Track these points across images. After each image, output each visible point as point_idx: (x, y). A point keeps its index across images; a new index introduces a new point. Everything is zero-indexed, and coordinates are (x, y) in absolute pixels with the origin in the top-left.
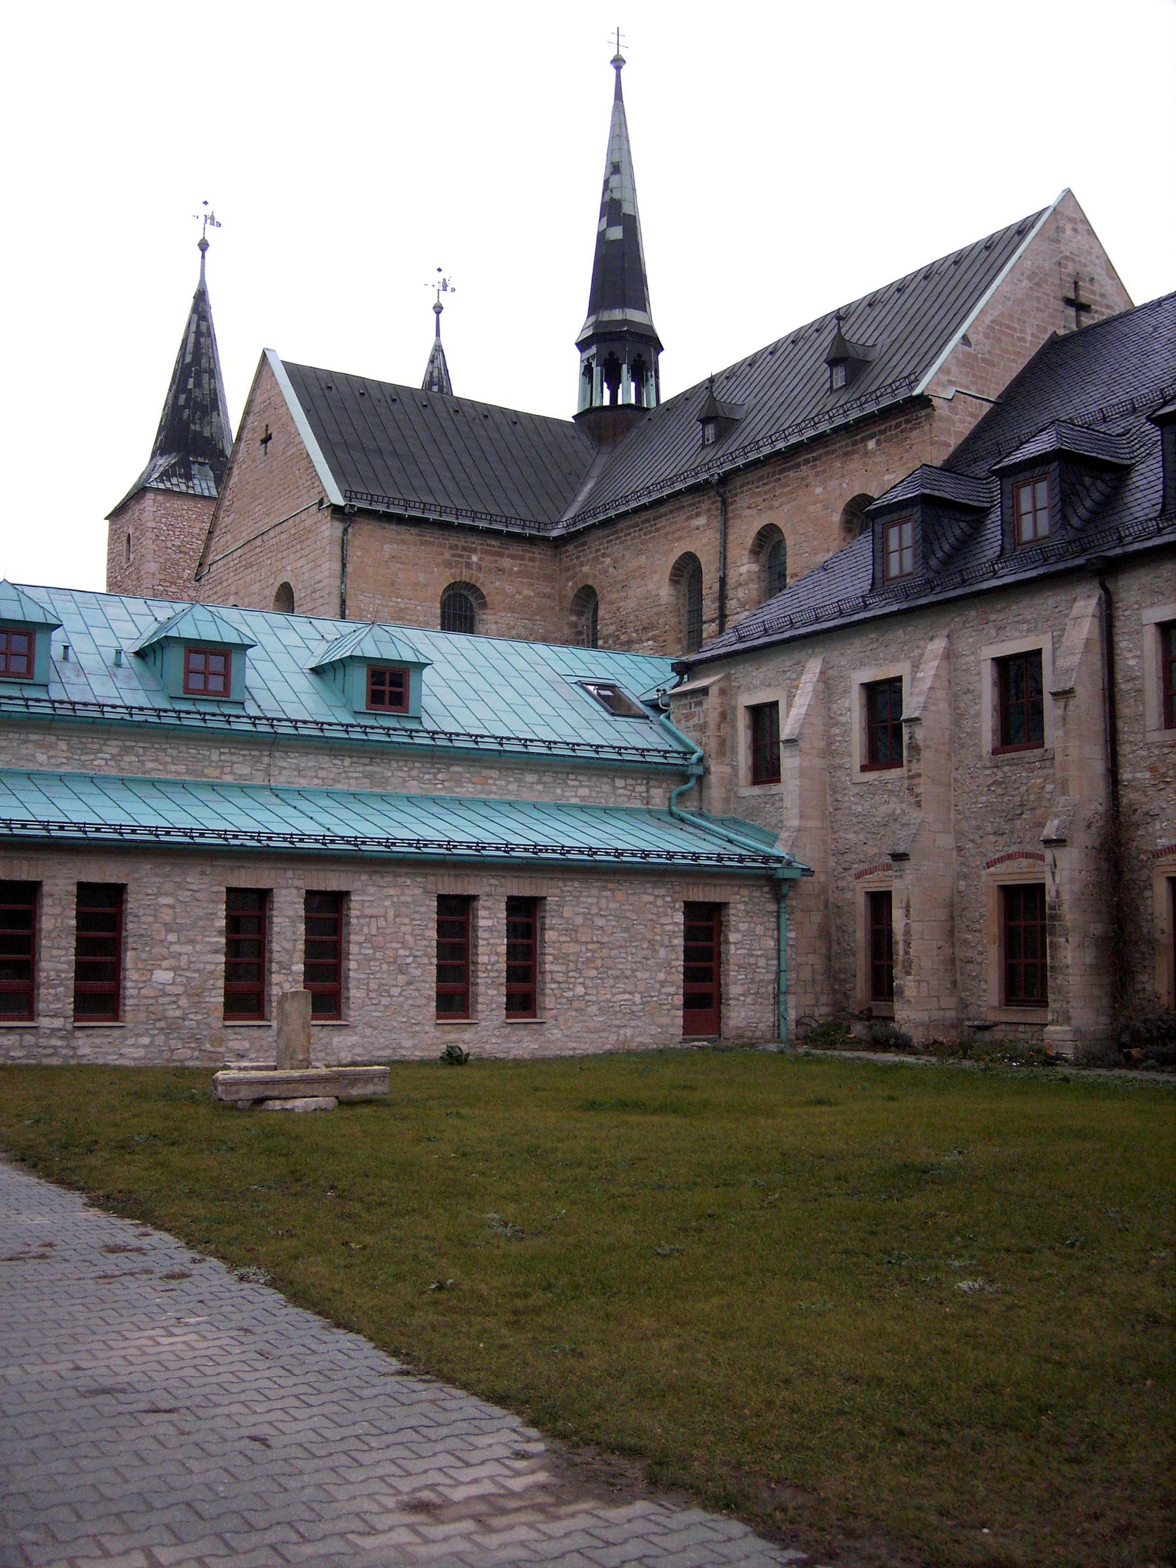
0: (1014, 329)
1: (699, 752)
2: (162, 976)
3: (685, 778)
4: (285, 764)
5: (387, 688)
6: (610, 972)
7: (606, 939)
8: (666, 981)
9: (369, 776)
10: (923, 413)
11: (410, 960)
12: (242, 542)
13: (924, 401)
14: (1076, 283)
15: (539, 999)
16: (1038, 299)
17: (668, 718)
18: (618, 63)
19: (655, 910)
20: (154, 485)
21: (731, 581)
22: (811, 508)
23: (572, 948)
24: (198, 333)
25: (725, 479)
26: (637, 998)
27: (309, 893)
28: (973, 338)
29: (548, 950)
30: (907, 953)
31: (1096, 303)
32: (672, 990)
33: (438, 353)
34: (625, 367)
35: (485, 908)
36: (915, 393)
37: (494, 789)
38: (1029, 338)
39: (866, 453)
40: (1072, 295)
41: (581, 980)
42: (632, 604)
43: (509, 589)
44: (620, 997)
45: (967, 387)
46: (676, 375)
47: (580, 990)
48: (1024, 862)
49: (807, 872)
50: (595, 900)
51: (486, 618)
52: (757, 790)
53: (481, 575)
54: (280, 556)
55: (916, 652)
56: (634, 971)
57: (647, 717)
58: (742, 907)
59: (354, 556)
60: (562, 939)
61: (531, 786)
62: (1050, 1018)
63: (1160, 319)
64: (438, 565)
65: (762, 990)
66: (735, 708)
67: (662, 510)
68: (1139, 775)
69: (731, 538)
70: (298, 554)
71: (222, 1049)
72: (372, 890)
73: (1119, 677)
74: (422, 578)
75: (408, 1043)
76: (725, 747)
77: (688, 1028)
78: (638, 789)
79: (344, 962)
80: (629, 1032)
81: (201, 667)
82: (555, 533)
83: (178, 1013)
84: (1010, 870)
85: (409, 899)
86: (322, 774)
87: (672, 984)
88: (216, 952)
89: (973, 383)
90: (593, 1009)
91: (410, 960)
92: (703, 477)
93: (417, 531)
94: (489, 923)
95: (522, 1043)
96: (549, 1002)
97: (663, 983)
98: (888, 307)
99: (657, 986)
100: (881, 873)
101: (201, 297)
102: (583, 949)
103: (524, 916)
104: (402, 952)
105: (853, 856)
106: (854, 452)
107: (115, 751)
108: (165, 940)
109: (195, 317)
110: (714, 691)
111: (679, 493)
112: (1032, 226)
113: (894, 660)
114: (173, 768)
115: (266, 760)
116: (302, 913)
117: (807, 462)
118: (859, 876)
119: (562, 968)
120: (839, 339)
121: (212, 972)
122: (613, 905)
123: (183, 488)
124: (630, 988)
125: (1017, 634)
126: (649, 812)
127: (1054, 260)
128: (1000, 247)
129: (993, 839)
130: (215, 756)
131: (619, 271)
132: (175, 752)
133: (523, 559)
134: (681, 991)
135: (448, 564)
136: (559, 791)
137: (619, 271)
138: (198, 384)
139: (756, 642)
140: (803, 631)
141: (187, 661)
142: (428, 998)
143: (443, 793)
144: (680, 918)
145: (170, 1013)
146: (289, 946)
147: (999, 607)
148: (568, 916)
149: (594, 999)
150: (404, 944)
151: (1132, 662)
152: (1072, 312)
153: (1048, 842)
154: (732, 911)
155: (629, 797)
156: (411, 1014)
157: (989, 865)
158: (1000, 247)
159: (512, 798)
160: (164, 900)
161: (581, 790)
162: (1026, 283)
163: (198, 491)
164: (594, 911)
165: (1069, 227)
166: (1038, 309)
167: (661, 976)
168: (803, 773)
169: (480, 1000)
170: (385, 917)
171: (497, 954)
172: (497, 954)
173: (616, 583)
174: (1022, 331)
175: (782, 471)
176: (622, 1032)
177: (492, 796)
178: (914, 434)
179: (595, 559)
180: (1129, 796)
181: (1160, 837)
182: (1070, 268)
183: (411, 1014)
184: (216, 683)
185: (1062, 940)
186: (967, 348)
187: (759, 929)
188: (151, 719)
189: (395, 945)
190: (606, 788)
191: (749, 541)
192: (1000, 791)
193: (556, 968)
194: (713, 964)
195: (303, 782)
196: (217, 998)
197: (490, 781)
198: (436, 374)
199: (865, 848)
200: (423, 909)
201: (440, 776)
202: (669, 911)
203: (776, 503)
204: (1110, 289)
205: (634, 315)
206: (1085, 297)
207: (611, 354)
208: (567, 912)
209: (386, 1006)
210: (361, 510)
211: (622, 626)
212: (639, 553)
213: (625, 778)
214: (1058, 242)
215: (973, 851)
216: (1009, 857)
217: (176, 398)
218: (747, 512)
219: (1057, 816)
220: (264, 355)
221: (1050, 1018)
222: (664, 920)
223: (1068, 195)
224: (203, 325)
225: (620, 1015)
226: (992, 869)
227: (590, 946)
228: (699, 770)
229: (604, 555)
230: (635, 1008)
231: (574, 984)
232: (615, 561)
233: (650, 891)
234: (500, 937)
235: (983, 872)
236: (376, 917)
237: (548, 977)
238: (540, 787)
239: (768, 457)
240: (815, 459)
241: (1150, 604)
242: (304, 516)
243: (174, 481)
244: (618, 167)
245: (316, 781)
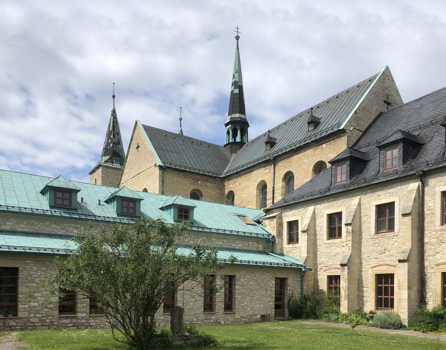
0: (370, 110)
5: (183, 214)
7: (253, 288)
12: (131, 177)
14: (388, 96)
15: (233, 306)
16: (377, 101)
17: (262, 225)
18: (237, 38)
20: (103, 164)
22: (303, 166)
23: (244, 291)
24: (114, 122)
28: (358, 111)
29: (236, 291)
31: (393, 103)
32: (272, 303)
34: (239, 131)
36: (341, 128)
39: (322, 148)
40: (386, 100)
46: (253, 133)
47: (246, 303)
48: (386, 267)
49: (310, 270)
50: (250, 277)
52: (291, 246)
54: (143, 181)
55: (348, 204)
56: (261, 298)
57: (256, 225)
59: (166, 180)
60: (241, 288)
63: (423, 103)
68: (432, 240)
70: (149, 180)
74: (185, 187)
76: (280, 233)
78: (255, 245)
79: (176, 295)
82: (222, 176)
84: (380, 269)
87: (272, 302)
92: (267, 158)
93: (183, 174)
96: (237, 307)
97: (269, 302)
98: (324, 107)
100: (333, 270)
103: (230, 281)
105: (323, 265)
109: (112, 117)
111: (261, 163)
112: (375, 78)
113: (340, 206)
118: (325, 271)
119: (241, 297)
120: (312, 116)
123: (111, 166)
124: (260, 303)
125: (386, 197)
128: (363, 86)
129: (374, 260)
131: (237, 101)
138: (114, 137)
139: (291, 203)
140: (315, 197)
141: (122, 204)
142: (201, 306)
147: (379, 189)
148: (243, 281)
151: (431, 204)
156: (196, 311)
158: (363, 86)
163: (115, 167)
165: (387, 78)
167: (268, 299)
169: (217, 306)
173: (240, 190)
174: (372, 110)
181: (440, 260)
182: (387, 91)
183: (196, 311)
184: (131, 211)
188: (111, 220)
191: (282, 176)
192: (377, 245)
193: (238, 297)
194: (282, 296)
199: (327, 263)
203: (291, 165)
204: (397, 99)
208: (242, 280)
211: (242, 202)
212: (247, 181)
215: (367, 264)
216: (380, 265)
217: (108, 141)
220: (136, 123)
222: (269, 283)
223: (387, 68)
226: (373, 269)
227: (248, 290)
229: (236, 182)
237: (236, 299)
239: (289, 151)
241: (439, 185)
242: (150, 169)
243: (108, 163)
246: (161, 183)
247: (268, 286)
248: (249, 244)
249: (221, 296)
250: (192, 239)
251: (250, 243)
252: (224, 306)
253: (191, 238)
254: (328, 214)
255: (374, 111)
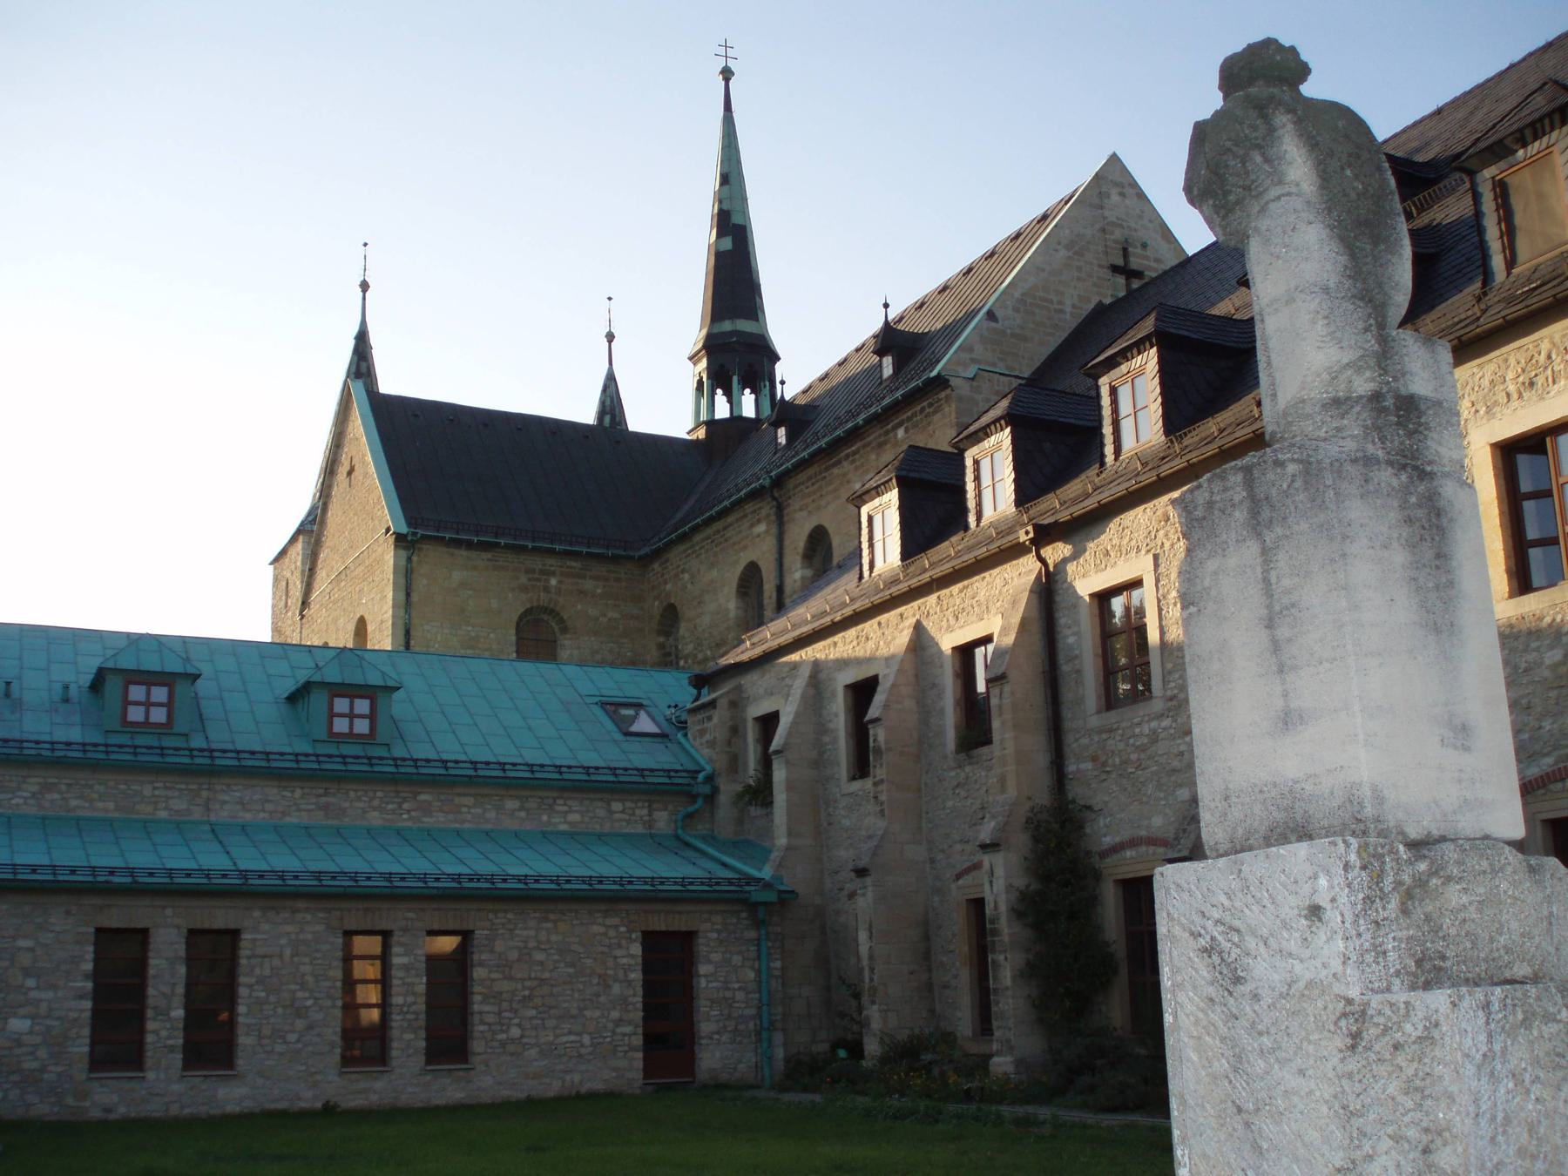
0: (1051, 301)
1: (708, 768)
2: (18, 1025)
3: (693, 798)
4: (226, 798)
6: (552, 1012)
7: (546, 975)
8: (621, 1020)
9: (325, 807)
10: (943, 395)
11: (309, 1003)
13: (941, 382)
14: (1125, 250)
16: (1079, 269)
17: (685, 735)
19: (607, 941)
21: (788, 589)
23: (506, 986)
25: (778, 482)
26: (586, 1040)
27: (192, 933)
28: (999, 313)
29: (477, 989)
30: (872, 980)
32: (628, 1029)
33: (610, 383)
35: (401, 944)
37: (469, 817)
38: (1068, 309)
40: (1120, 262)
41: (516, 1021)
42: (706, 620)
43: (592, 612)
44: (564, 1039)
45: (994, 365)
47: (515, 1032)
50: (532, 933)
51: (567, 646)
53: (561, 600)
58: (715, 935)
59: (420, 583)
61: (511, 813)
62: (995, 1047)
64: (513, 590)
65: (741, 1027)
66: (744, 720)
67: (730, 519)
69: (787, 543)
71: (87, 1104)
72: (266, 927)
73: (1062, 657)
75: (308, 1094)
77: (648, 1071)
78: (638, 812)
80: (577, 1078)
81: (142, 698)
83: (35, 1065)
85: (309, 936)
86: (269, 807)
87: (630, 1023)
88: (81, 997)
89: (1001, 360)
90: (533, 1052)
91: (309, 1003)
93: (489, 555)
94: (405, 960)
95: (448, 1089)
99: (610, 1025)
101: (362, 339)
102: (519, 986)
104: (300, 994)
106: (885, 443)
107: (35, 788)
108: (22, 986)
110: (723, 703)
114: (100, 805)
115: (205, 794)
116: (182, 953)
117: (847, 456)
121: (76, 1020)
122: (554, 938)
126: (652, 836)
127: (1097, 226)
130: (147, 791)
131: (734, 282)
132: (102, 789)
133: (607, 580)
134: (640, 1031)
135: (524, 589)
136: (545, 818)
137: (734, 282)
142: (332, 1045)
143: (409, 824)
144: (637, 949)
145: (26, 1066)
146: (166, 989)
148: (509, 950)
149: (533, 1041)
150: (303, 986)
152: (1121, 280)
153: (984, 847)
154: (701, 941)
155: (628, 822)
157: (958, 877)
159: (488, 827)
160: (22, 943)
161: (570, 815)
162: (1063, 253)
164: (532, 944)
166: (1079, 279)
167: (615, 1014)
168: (790, 786)
170: (281, 956)
171: (414, 994)
172: (414, 994)
174: (1060, 303)
175: (827, 469)
176: (568, 1078)
177: (466, 825)
178: (937, 417)
179: (676, 576)
180: (1075, 791)
182: (1118, 234)
185: (1002, 957)
186: (993, 324)
187: (737, 959)
189: (293, 987)
190: (601, 813)
192: (963, 794)
193: (486, 1008)
195: (248, 816)
196: (81, 1047)
197: (464, 809)
198: (608, 403)
200: (325, 947)
201: (405, 806)
202: (624, 942)
203: (823, 503)
205: (745, 326)
206: (1135, 263)
207: (722, 366)
208: (499, 946)
209: (281, 1054)
210: (423, 537)
212: (712, 566)
213: (622, 801)
214: (1102, 207)
218: (798, 515)
219: (994, 817)
221: (995, 1047)
224: (364, 365)
225: (565, 1059)
226: (961, 882)
227: (528, 984)
228: (707, 789)
229: (683, 571)
230: (583, 1051)
231: (509, 1026)
232: (692, 576)
233: (600, 920)
234: (418, 975)
235: (953, 886)
236: (271, 956)
237: (476, 1019)
238: (523, 814)
240: (854, 453)
244: (730, 177)
245: (262, 815)
246: (402, 596)
247: (610, 963)
248: (611, 812)
249: (414, 1008)
250: (376, 803)
251: (617, 806)
252: (424, 1044)
253: (371, 800)
254: (847, 687)
255: (1068, 302)
